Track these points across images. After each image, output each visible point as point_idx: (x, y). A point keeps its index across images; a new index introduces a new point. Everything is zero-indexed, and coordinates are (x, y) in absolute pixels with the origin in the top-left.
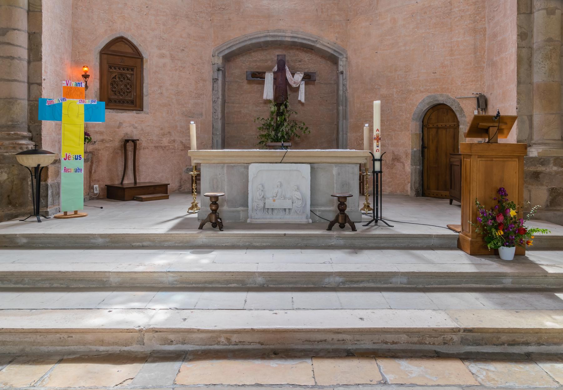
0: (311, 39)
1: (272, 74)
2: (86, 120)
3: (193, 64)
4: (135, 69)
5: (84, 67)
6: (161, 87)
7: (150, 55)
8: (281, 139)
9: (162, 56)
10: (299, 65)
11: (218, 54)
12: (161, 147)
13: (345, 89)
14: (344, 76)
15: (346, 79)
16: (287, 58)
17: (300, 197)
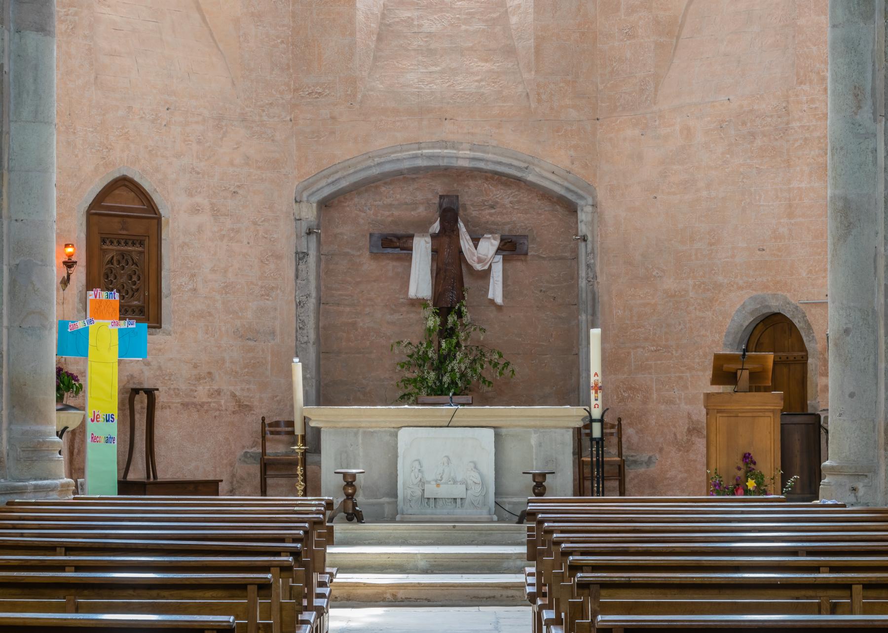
0: (516, 163)
1: (429, 239)
2: (121, 355)
3: (255, 223)
4: (146, 242)
5: (67, 246)
6: (193, 275)
7: (173, 210)
8: (449, 389)
9: (196, 210)
10: (491, 215)
11: (308, 197)
12: (195, 404)
13: (591, 275)
14: (589, 246)
15: (593, 252)
16: (465, 199)
17: (478, 480)
